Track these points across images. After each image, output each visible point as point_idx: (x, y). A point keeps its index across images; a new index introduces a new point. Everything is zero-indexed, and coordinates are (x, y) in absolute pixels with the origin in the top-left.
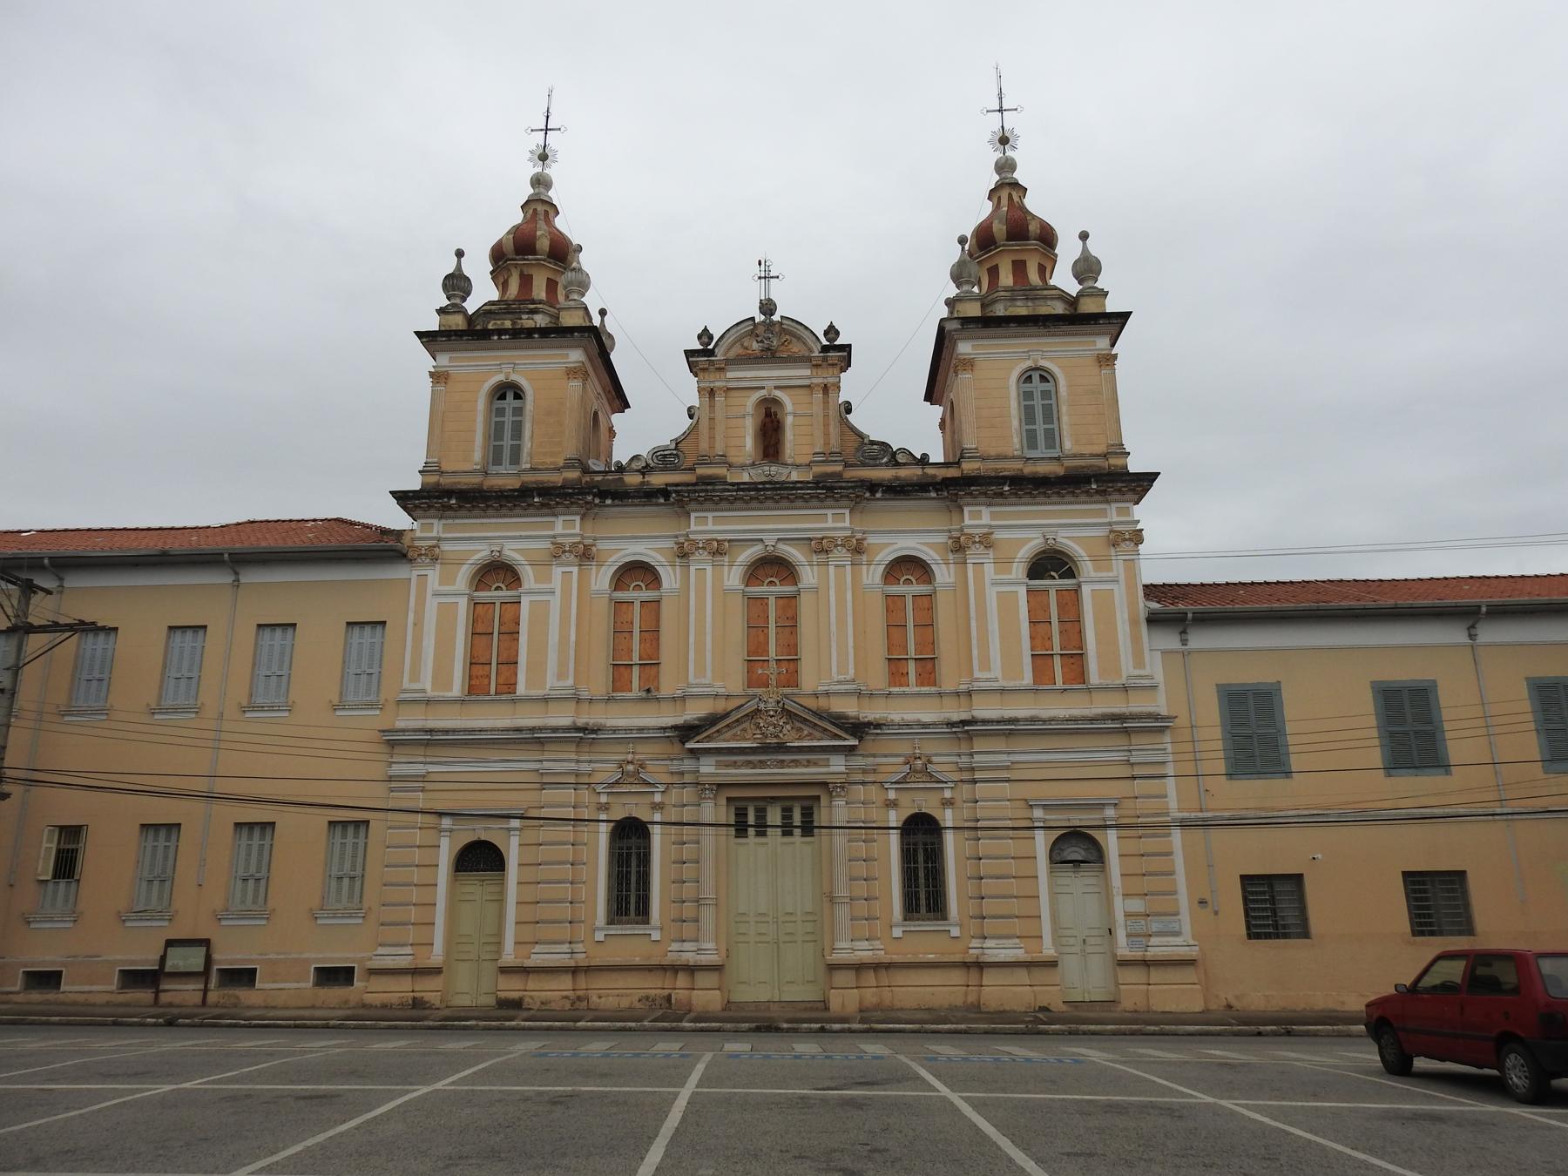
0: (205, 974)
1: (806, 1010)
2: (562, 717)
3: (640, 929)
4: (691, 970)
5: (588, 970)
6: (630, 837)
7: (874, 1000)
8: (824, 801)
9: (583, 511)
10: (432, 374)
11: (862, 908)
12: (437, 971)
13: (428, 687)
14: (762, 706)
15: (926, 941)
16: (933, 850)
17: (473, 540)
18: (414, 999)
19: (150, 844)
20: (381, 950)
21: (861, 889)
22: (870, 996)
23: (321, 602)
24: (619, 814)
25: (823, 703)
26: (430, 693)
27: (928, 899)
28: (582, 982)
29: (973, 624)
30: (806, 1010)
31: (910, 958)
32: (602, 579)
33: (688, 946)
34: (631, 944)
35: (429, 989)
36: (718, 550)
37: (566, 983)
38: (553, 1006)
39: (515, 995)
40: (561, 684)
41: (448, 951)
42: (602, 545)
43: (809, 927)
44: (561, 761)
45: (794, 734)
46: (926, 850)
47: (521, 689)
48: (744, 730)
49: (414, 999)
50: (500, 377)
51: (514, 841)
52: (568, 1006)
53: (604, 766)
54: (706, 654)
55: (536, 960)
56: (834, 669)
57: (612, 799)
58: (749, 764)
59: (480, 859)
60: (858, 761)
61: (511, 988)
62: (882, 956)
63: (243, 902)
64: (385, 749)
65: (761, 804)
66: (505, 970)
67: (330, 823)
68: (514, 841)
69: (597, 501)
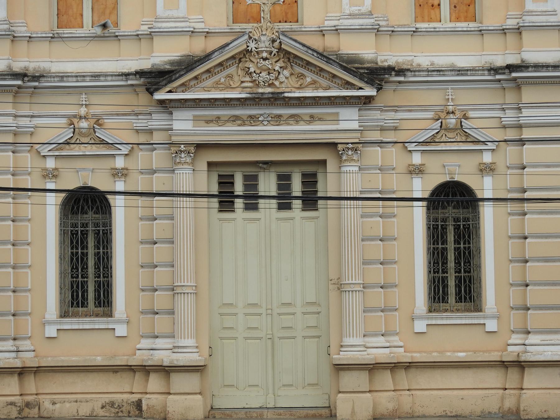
3: (101, 323)
5: (38, 371)
6: (86, 209)
7: (391, 406)
14: (252, 45)
15: (456, 335)
16: (467, 228)
27: (458, 286)
28: (31, 384)
31: (435, 357)
43: (312, 320)
45: (293, 82)
46: (457, 228)
57: (61, 164)
65: (250, 171)
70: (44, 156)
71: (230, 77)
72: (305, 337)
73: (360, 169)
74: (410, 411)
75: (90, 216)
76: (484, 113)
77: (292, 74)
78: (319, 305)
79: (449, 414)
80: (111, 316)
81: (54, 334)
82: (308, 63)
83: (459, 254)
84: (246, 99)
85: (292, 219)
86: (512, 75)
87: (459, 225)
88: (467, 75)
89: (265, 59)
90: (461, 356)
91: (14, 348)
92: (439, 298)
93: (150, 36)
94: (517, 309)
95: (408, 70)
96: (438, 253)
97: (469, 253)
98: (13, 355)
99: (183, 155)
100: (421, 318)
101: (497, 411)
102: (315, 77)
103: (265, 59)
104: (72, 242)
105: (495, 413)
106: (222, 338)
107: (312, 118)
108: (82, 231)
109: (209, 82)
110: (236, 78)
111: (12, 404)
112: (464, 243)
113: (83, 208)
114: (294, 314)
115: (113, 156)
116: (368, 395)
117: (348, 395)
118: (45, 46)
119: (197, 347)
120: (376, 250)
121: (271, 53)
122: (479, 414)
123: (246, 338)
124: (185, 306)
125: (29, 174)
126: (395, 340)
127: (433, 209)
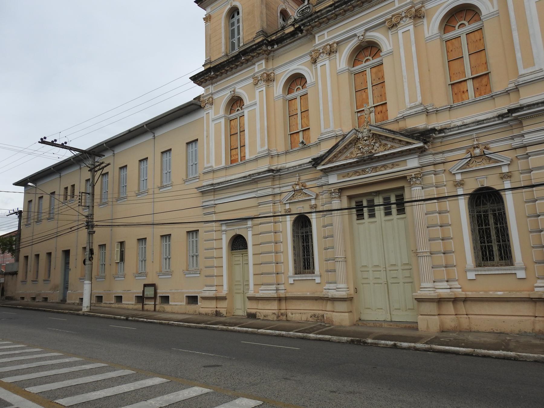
0: (155, 298)
1: (405, 328)
2: (263, 166)
3: (309, 277)
4: (334, 300)
5: (286, 299)
6: (302, 223)
7: (453, 324)
8: (406, 190)
9: (265, 56)
10: (204, 19)
11: (441, 259)
12: (224, 298)
13: (214, 165)
14: (360, 135)
15: (495, 281)
16: (500, 214)
17: (222, 91)
18: (216, 311)
19: (165, 243)
20: (206, 288)
21: (439, 246)
22: (450, 321)
23: (174, 136)
24: (472, 186)
25: (402, 125)
26: (215, 167)
27: (500, 250)
28: (283, 305)
29: (515, 35)
30: (405, 328)
31: (482, 294)
32: (278, 88)
33: (332, 286)
34: (305, 286)
35: (222, 307)
36: (331, 51)
37: (274, 306)
38: (270, 318)
39: (253, 311)
40: (263, 149)
41: (230, 289)
42: (277, 72)
43: (407, 274)
44: (266, 188)
45: (382, 149)
46: (494, 215)
47: (247, 157)
48: (352, 153)
49: (216, 311)
50: (229, 7)
51: (250, 233)
52: (275, 319)
53: (286, 186)
54: (331, 113)
55: (261, 294)
56: (407, 100)
57: (465, 176)
58: (356, 172)
59: (238, 243)
60: (429, 159)
61: (252, 307)
62: (460, 293)
63: (166, 268)
64: (200, 195)
65: (370, 198)
66: (250, 298)
67: (188, 232)
68: (250, 233)
69: (269, 48)
70: (454, 174)
71: (352, 153)
72: (404, 283)
73: (423, 188)
74: (468, 328)
75: (489, 206)
76: (499, 144)
77: (380, 145)
78: (411, 265)
79: (495, 331)
80: (512, 265)
81: (474, 278)
82: (387, 137)
83: (498, 231)
84: (357, 162)
85: (392, 220)
86: (514, 117)
87: (496, 214)
88: (484, 123)
89: (366, 141)
90: (500, 294)
91: (449, 287)
92: (487, 258)
93: (516, 89)
94: (539, 263)
95: (446, 129)
96: (483, 232)
97: (504, 229)
98: (275, 291)
99: (333, 194)
100: (470, 270)
101: (531, 332)
102: (392, 144)
103: (366, 141)
104: (478, 222)
105: (530, 333)
106: (363, 284)
107: (393, 165)
108: (484, 215)
109: (343, 157)
110: (354, 153)
111: (274, 314)
112: (500, 224)
113: (483, 201)
114: (397, 270)
115: (500, 166)
116: (437, 317)
117: (424, 317)
118: (447, 113)
119: (348, 288)
120: (438, 232)
121: (369, 137)
122: (517, 332)
123: (375, 284)
124: (340, 267)
125: (445, 186)
126: (456, 284)
127: (476, 206)
